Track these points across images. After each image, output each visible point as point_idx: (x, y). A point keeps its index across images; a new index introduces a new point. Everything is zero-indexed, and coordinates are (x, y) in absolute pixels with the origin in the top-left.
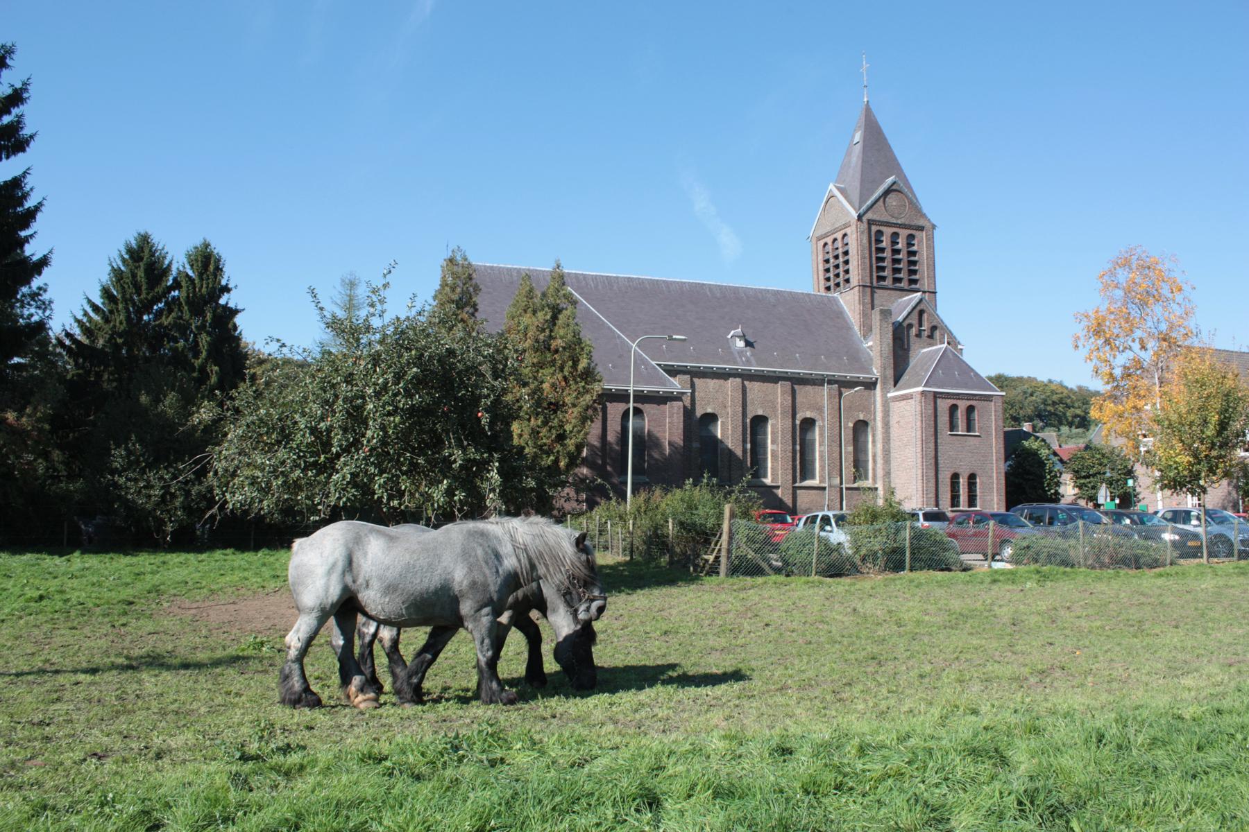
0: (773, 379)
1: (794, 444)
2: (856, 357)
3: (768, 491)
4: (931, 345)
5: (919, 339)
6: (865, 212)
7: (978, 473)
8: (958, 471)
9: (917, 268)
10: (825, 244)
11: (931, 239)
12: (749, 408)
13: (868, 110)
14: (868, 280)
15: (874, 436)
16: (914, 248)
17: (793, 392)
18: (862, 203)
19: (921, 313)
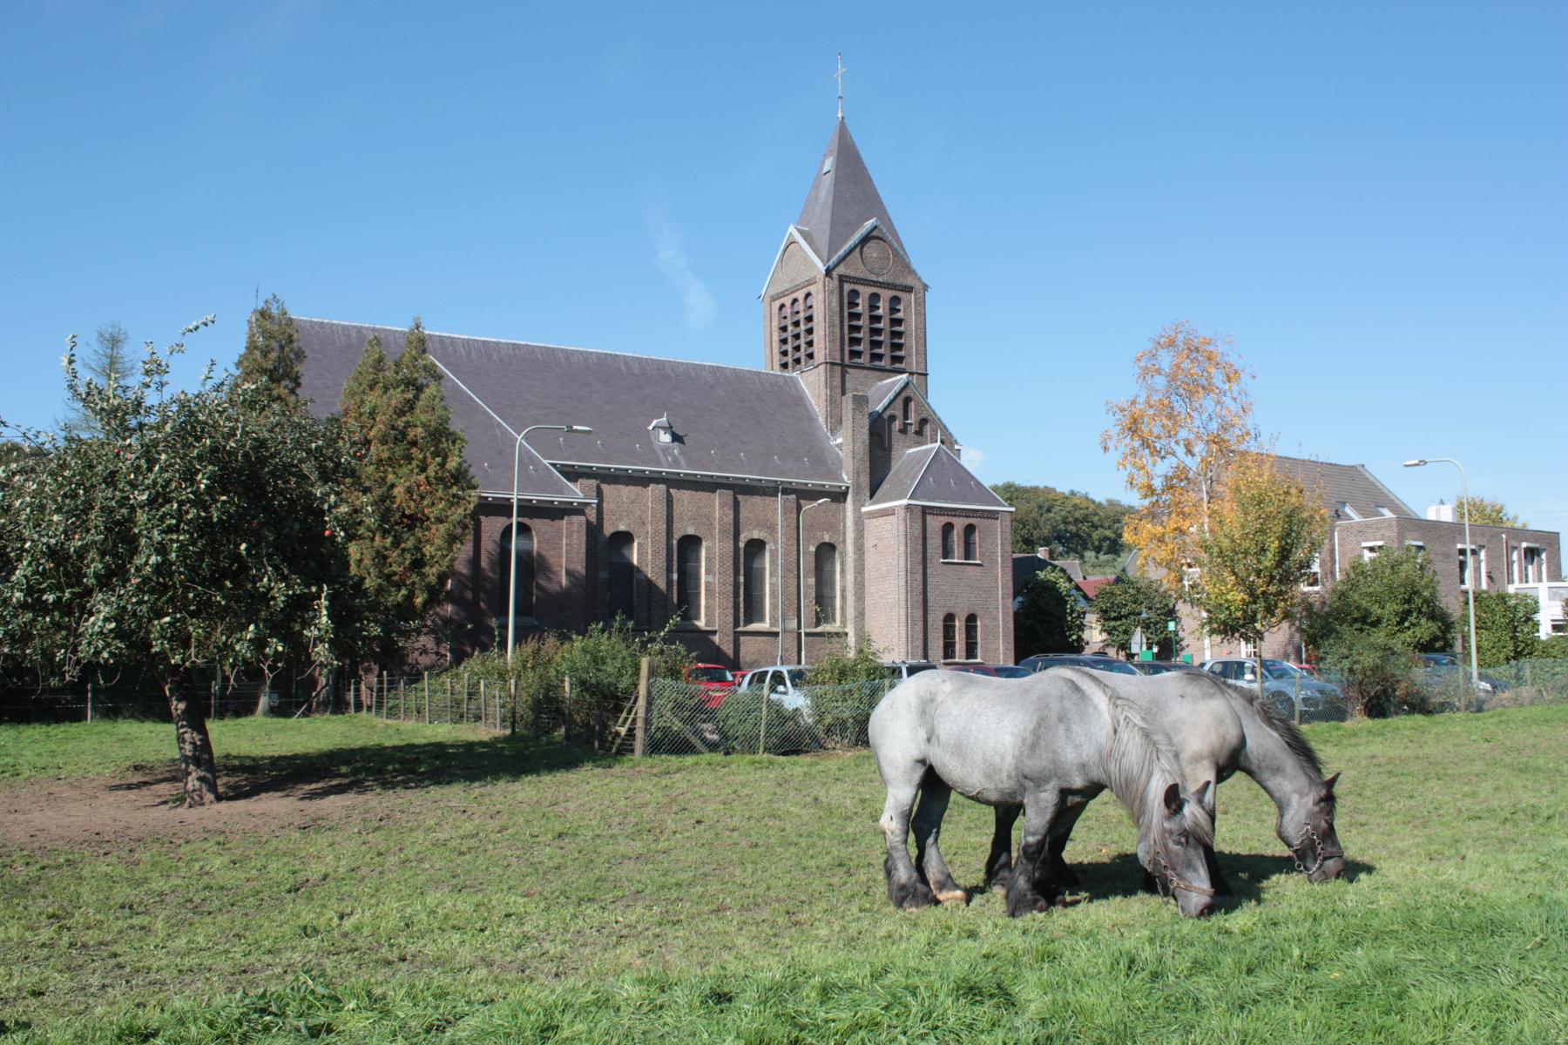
1: (736, 574)
2: (821, 459)
4: (920, 444)
5: (903, 436)
7: (979, 613)
8: (951, 611)
9: (902, 341)
10: (782, 306)
11: (921, 304)
12: (676, 525)
13: (843, 129)
14: (837, 355)
15: (843, 564)
16: (900, 315)
17: (736, 506)
18: (831, 252)
19: (907, 401)
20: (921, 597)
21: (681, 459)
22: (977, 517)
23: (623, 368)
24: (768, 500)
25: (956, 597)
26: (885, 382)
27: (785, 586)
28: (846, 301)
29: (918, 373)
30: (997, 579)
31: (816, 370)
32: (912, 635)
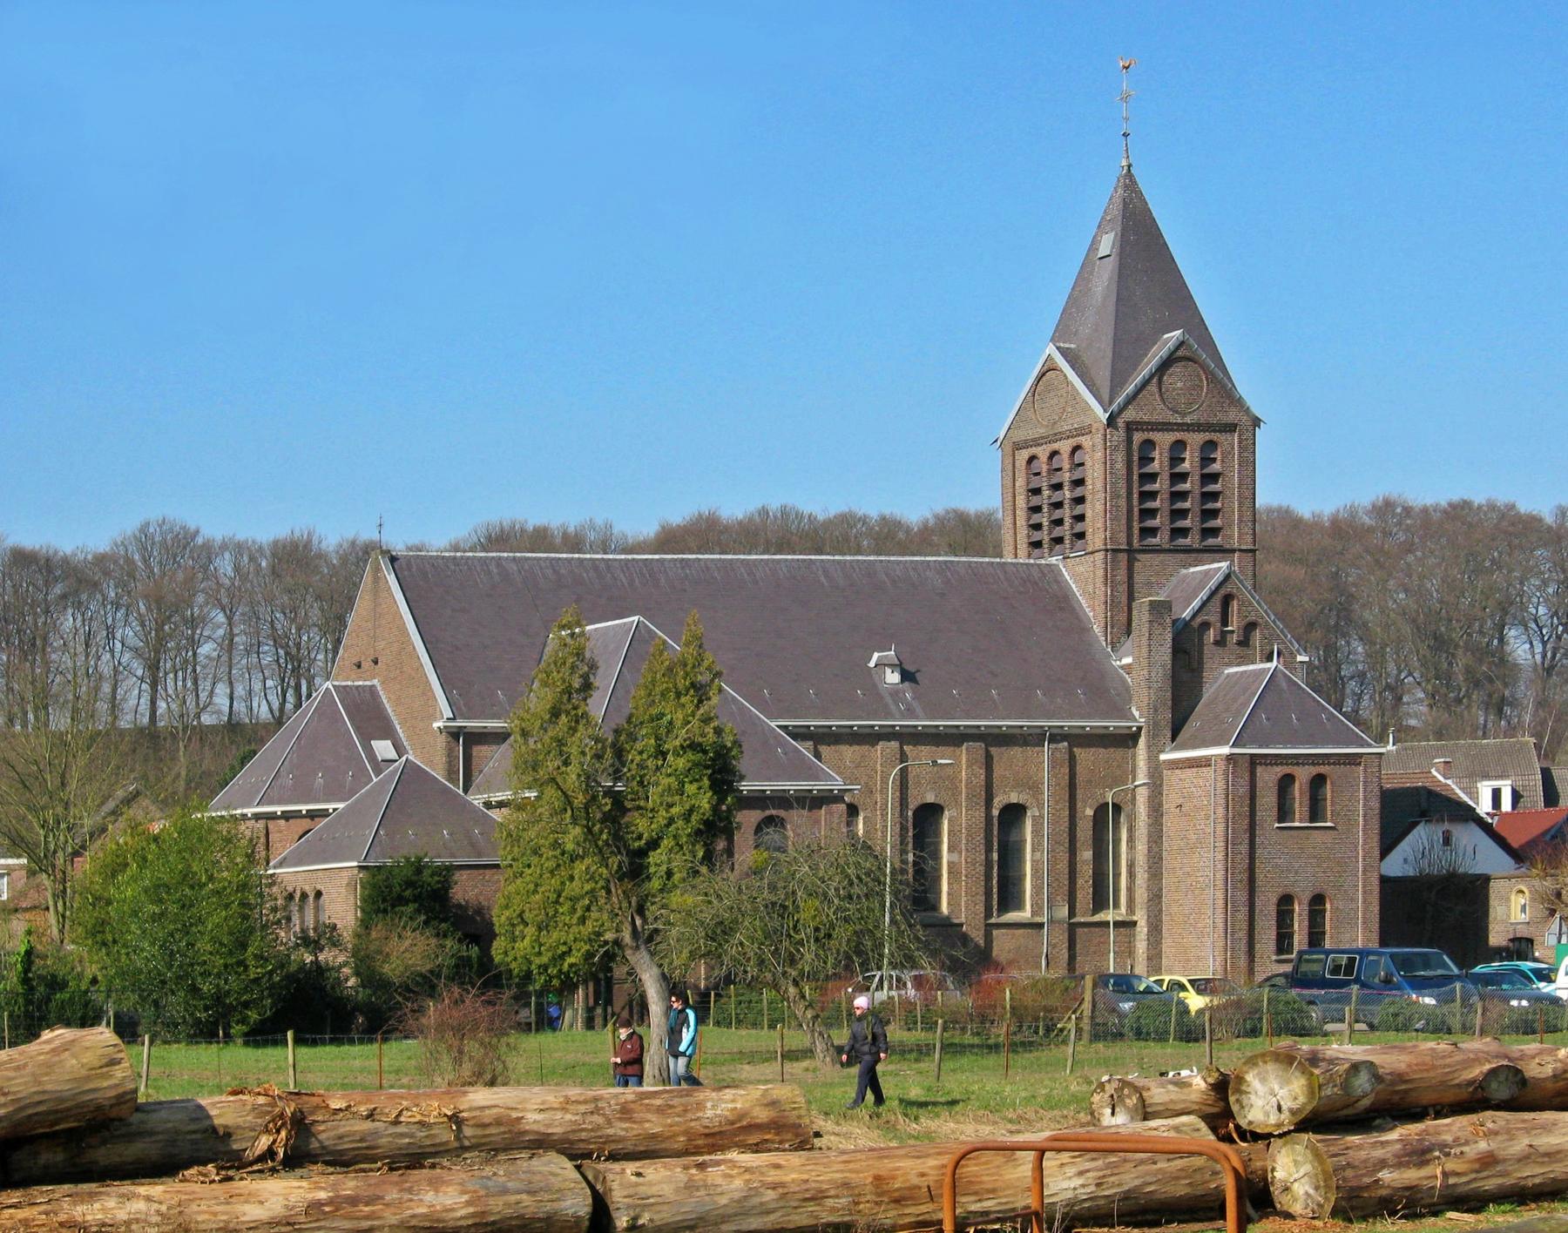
0: (953, 738)
1: (989, 850)
2: (1106, 694)
3: (948, 928)
4: (1243, 660)
5: (1220, 650)
6: (1121, 410)
7: (1329, 892)
8: (1289, 890)
9: (1219, 505)
10: (1032, 459)
11: (1249, 448)
12: (912, 792)
13: (1129, 182)
14: (1123, 537)
15: (1131, 830)
16: (1216, 467)
17: (989, 761)
18: (1117, 381)
19: (1227, 600)
20: (1246, 875)
21: (915, 704)
22: (1329, 764)
23: (822, 579)
24: (1030, 751)
25: (1296, 873)
26: (1192, 570)
27: (1052, 862)
28: (1136, 458)
29: (1241, 550)
30: (1356, 847)
31: (1090, 558)
32: (1233, 925)
